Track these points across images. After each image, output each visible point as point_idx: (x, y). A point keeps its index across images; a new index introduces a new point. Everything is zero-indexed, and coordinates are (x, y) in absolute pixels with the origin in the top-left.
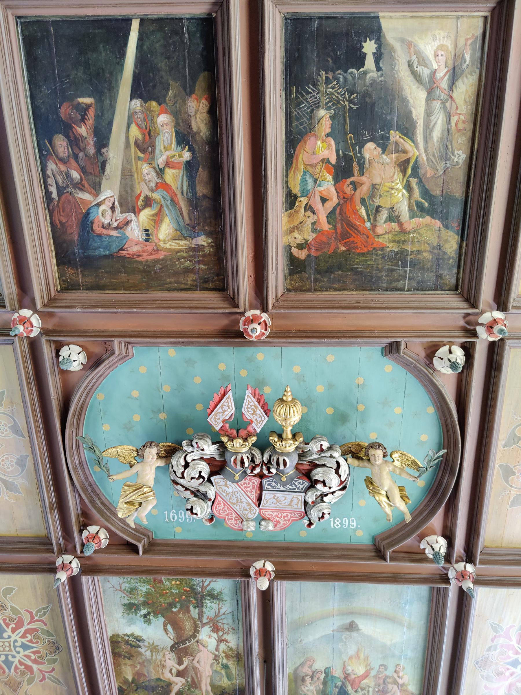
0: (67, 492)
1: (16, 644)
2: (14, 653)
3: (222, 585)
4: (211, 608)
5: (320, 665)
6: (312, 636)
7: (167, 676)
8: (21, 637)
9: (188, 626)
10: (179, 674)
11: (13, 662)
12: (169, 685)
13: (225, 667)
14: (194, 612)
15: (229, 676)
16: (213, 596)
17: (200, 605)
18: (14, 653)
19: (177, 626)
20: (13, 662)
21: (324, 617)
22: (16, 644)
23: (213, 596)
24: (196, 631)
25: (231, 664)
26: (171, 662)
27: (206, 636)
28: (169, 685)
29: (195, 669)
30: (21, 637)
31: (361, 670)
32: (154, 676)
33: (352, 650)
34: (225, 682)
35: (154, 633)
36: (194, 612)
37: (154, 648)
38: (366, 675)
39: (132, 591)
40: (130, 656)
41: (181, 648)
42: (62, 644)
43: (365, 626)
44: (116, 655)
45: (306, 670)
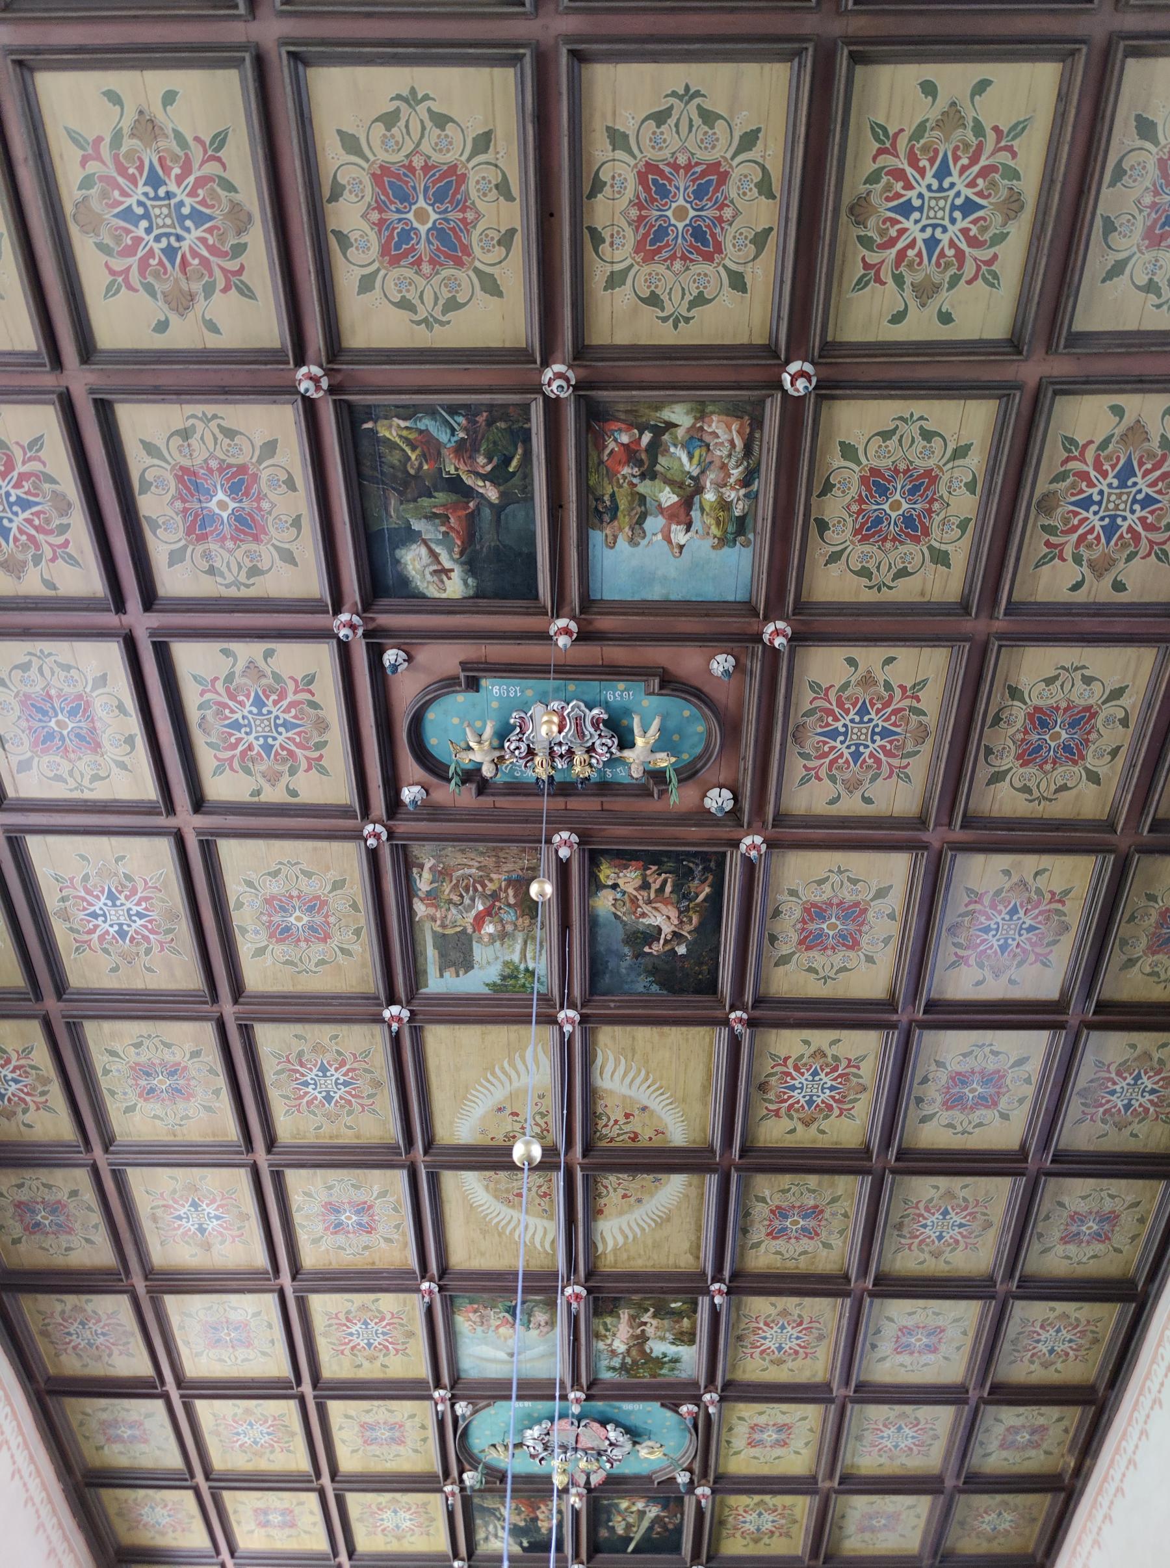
0: (562, 273)
1: (939, 230)
2: (952, 193)
3: (606, 1375)
4: (616, 1362)
5: (534, 1333)
6: (541, 1349)
7: (655, 1322)
8: (923, 177)
9: (634, 1352)
10: (645, 1324)
11: (967, 198)
12: (654, 1316)
13: (607, 1330)
14: (628, 1360)
15: (605, 1324)
16: (614, 1369)
17: (623, 1364)
18: (952, 193)
19: (643, 1352)
20: (967, 198)
21: (532, 1360)
22: (939, 230)
23: (614, 1369)
24: (628, 1351)
25: (603, 1332)
26: (650, 1331)
27: (620, 1346)
28: (654, 1316)
29: (632, 1327)
30: (923, 177)
31: (502, 1330)
32: (666, 1322)
33: (510, 1342)
34: (609, 1320)
35: (659, 1347)
36: (628, 1360)
37: (663, 1339)
38: (498, 1327)
39: (673, 1369)
40: (682, 1333)
41: (643, 1338)
42: (731, 1340)
43: (502, 1355)
44: (694, 1334)
45: (545, 1330)
